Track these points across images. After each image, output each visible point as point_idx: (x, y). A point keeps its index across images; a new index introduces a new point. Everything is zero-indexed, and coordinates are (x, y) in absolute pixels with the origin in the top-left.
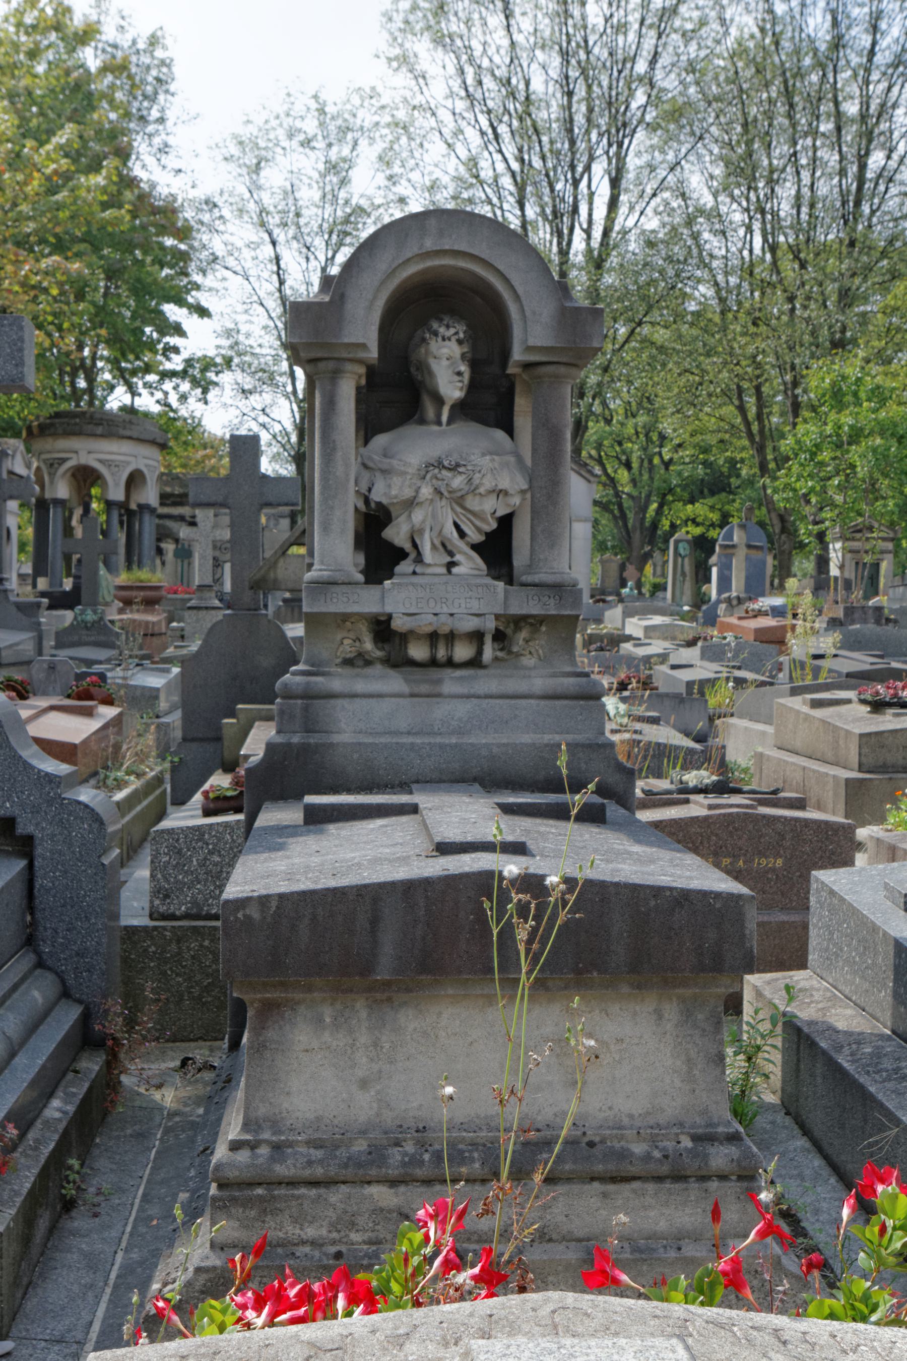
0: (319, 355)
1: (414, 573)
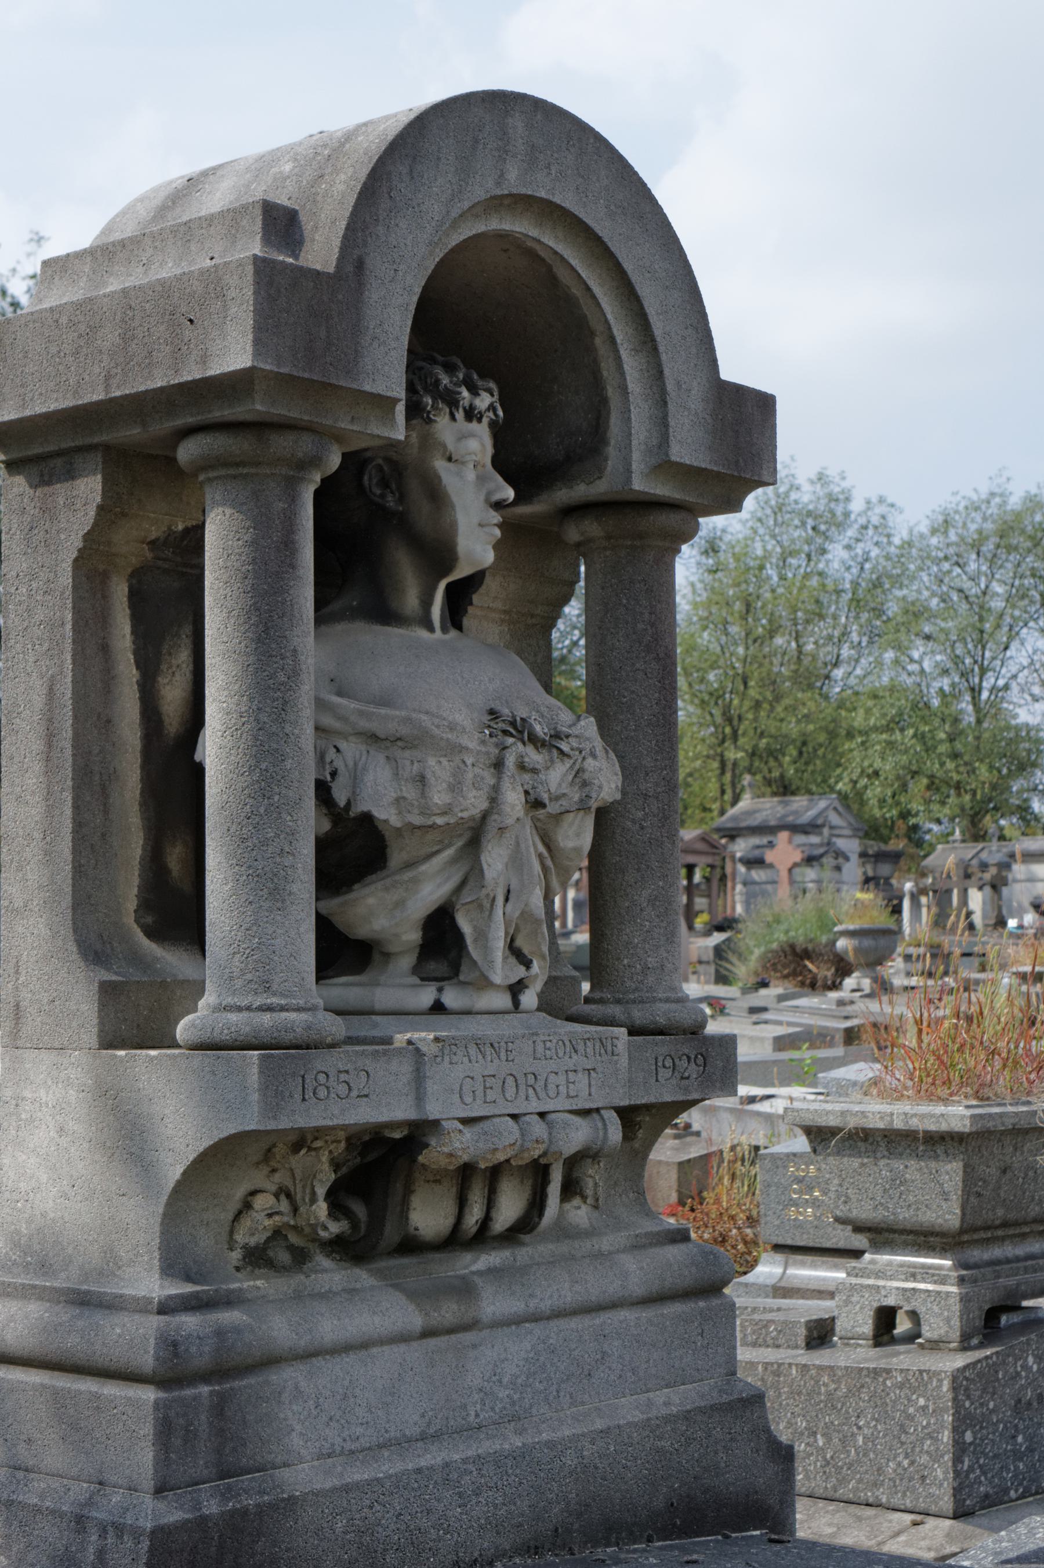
0: (294, 414)
1: (438, 1008)
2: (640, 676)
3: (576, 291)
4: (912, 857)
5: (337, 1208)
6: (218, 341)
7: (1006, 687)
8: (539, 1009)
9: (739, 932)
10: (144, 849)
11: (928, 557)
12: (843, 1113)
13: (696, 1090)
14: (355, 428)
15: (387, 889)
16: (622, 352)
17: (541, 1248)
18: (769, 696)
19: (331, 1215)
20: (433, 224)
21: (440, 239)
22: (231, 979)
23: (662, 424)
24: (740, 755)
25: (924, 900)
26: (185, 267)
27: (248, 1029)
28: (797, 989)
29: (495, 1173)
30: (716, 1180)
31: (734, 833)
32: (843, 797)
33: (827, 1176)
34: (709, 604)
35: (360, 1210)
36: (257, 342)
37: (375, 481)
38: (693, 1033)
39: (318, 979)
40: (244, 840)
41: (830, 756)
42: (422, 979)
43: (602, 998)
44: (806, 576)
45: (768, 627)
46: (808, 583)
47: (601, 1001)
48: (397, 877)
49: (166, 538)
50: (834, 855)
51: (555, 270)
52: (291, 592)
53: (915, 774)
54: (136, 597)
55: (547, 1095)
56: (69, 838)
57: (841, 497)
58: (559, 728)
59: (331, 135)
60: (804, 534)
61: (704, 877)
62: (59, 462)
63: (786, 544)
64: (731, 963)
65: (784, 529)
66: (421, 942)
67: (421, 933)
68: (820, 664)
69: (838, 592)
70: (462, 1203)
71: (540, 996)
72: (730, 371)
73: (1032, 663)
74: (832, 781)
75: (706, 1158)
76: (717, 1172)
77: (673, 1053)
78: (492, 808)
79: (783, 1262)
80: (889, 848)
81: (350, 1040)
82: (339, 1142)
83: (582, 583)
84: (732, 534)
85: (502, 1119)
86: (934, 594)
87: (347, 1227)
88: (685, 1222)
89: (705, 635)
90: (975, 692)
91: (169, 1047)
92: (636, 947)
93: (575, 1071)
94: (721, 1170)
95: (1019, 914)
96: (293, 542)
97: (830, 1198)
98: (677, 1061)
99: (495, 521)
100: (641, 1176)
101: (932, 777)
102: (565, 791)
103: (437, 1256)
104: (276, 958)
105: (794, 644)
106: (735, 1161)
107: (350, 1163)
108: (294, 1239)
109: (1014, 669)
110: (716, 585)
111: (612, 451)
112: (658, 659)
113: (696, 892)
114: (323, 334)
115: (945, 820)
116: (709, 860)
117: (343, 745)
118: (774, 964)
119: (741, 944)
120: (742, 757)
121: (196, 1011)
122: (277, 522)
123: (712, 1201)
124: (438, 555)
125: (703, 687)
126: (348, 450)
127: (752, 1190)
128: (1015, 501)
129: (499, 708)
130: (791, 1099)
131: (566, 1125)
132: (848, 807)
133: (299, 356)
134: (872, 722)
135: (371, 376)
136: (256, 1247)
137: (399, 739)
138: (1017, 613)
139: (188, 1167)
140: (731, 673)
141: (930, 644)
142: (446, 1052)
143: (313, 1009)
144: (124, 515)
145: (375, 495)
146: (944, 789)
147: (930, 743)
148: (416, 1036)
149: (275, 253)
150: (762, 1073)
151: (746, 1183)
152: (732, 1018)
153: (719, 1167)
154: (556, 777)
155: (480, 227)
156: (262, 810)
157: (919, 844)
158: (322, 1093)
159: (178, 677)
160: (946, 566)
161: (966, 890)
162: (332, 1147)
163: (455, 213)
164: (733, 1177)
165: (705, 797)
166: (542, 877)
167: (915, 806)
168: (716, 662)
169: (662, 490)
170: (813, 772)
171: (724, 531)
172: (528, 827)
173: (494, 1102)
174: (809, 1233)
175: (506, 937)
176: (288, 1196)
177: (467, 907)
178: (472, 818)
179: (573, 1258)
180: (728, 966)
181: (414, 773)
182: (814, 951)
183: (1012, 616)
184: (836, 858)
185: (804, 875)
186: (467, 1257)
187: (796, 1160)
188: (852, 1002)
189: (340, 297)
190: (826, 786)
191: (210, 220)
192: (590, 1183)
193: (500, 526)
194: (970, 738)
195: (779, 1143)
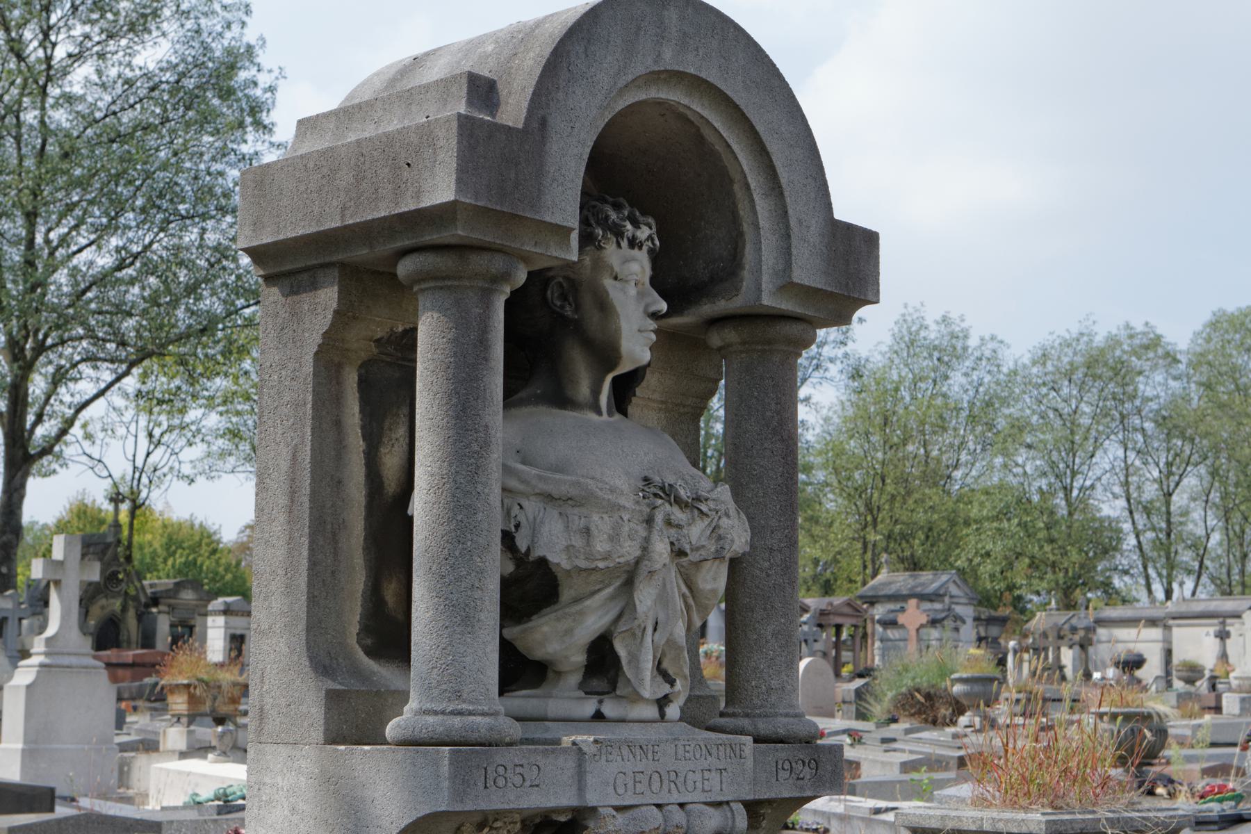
0: (488, 238)
1: (599, 716)
2: (768, 453)
3: (719, 147)
4: (1017, 622)
7: (1092, 487)
8: (681, 720)
9: (875, 678)
10: (366, 585)
11: (1030, 383)
12: (943, 818)
14: (538, 250)
15: (558, 620)
22: (430, 688)
23: (787, 252)
24: (879, 537)
25: (1026, 656)
32: (961, 572)
36: (459, 181)
39: (501, 694)
40: (442, 577)
41: (950, 540)
42: (586, 693)
44: (933, 396)
47: (734, 715)
48: (567, 610)
53: (1018, 555)
54: (364, 384)
56: (305, 574)
57: (961, 335)
59: (525, 24)
62: (305, 276)
69: (958, 410)
72: (840, 214)
73: (1113, 467)
74: (952, 559)
80: (998, 615)
86: (1034, 412)
90: (1067, 490)
95: (1104, 666)
96: (487, 340)
99: (652, 328)
101: (1032, 557)
105: (922, 451)
109: (1099, 473)
110: (861, 403)
111: (746, 274)
113: (842, 646)
114: (513, 176)
115: (1043, 593)
116: (854, 621)
117: (525, 503)
128: (1099, 340)
132: (965, 581)
134: (985, 512)
138: (1101, 428)
141: (1032, 452)
142: (604, 751)
143: (495, 714)
144: (355, 318)
146: (1042, 567)
147: (1031, 531)
154: (697, 532)
155: (642, 96)
156: (457, 553)
157: (1023, 611)
158: (501, 782)
160: (1044, 390)
161: (1059, 648)
163: (621, 84)
167: (1019, 581)
171: (867, 360)
178: (627, 563)
183: (1097, 431)
185: (929, 635)
188: (966, 735)
190: (946, 563)
191: (427, 88)
193: (655, 332)
194: (1063, 528)
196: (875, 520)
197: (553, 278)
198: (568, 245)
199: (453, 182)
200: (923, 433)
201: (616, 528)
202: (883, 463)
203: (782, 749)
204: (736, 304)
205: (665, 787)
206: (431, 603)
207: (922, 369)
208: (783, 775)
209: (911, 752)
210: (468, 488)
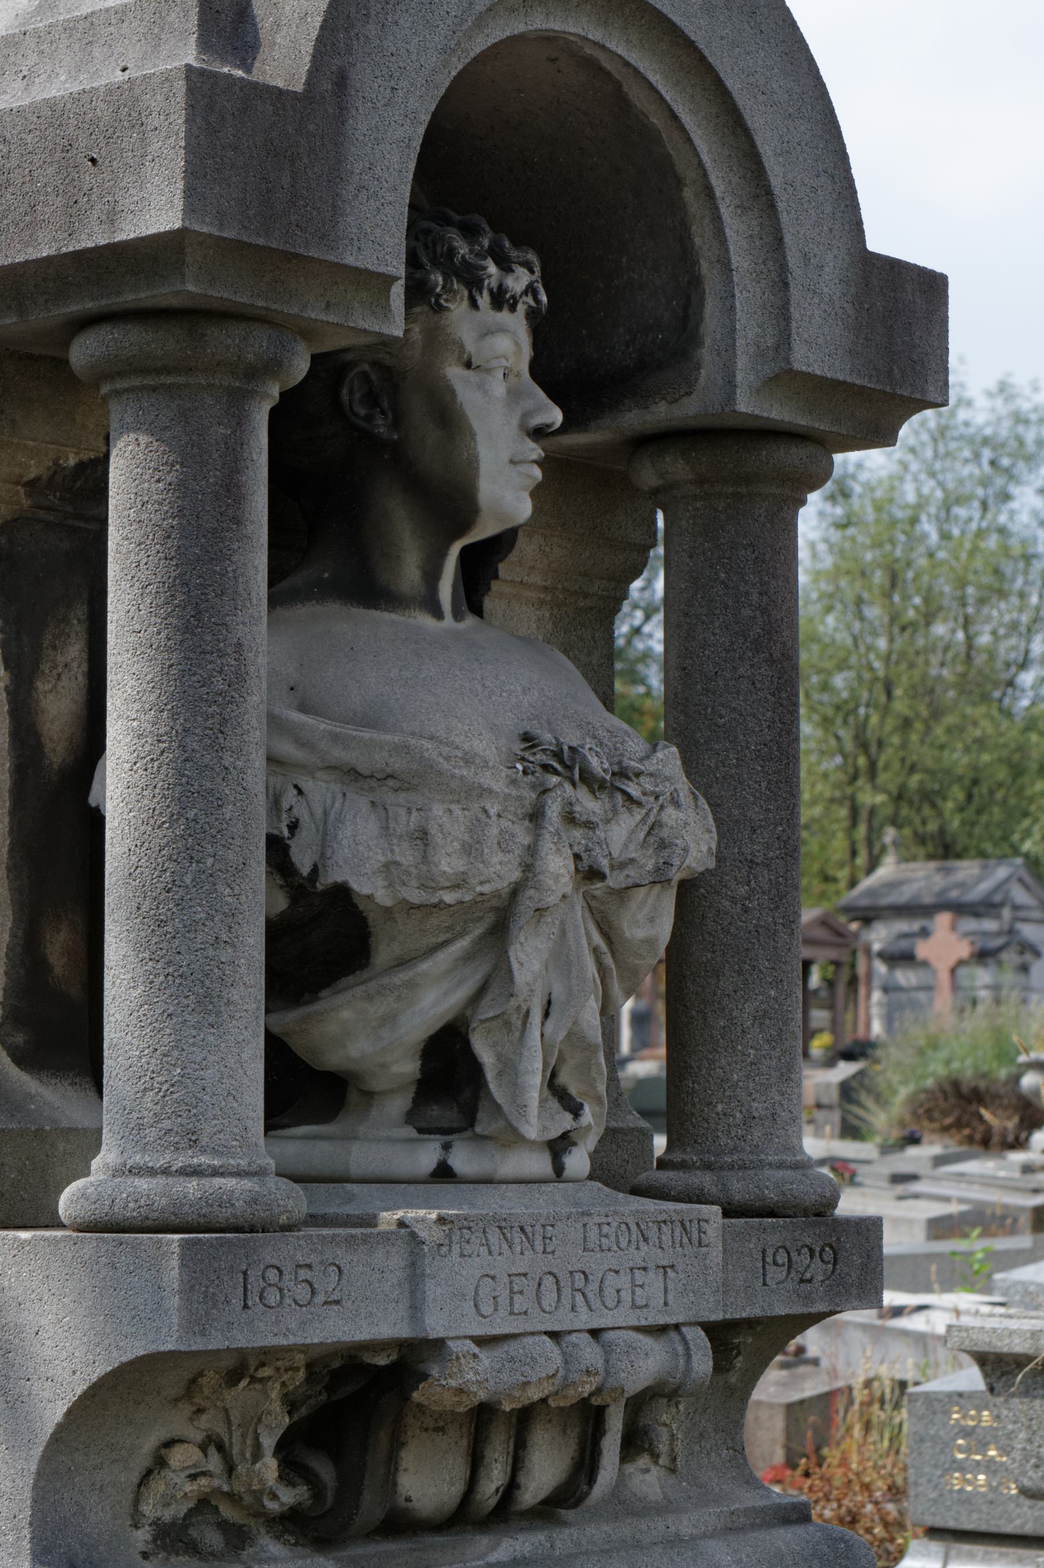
1: (443, 1173)
3: (657, 120)
5: (291, 1467)
6: (132, 191)
8: (591, 1177)
9: (877, 1061)
10: (13, 935)
13: (822, 1299)
14: (332, 318)
15: (370, 998)
16: (722, 210)
17: (590, 1530)
18: (924, 712)
19: (283, 1478)
20: (449, 22)
21: (459, 43)
22: (140, 1127)
24: (880, 798)
26: (84, 82)
27: (164, 1201)
28: (964, 1148)
29: (525, 1418)
30: (842, 1430)
31: (871, 914)
33: (1010, 1427)
34: (837, 572)
35: (325, 1471)
36: (189, 193)
37: (357, 396)
38: (818, 1215)
40: (161, 924)
41: (1013, 801)
42: (420, 1131)
43: (683, 1161)
44: (980, 534)
45: (923, 609)
46: (982, 545)
47: (683, 1166)
48: (385, 981)
49: (51, 478)
50: (1019, 948)
51: (625, 88)
52: (234, 559)
55: (604, 1304)
58: (626, 762)
60: (977, 472)
61: (824, 979)
63: (951, 486)
64: (864, 1107)
65: (948, 463)
66: (419, 1076)
67: (420, 1062)
68: (999, 665)
70: (476, 1462)
71: (593, 1156)
72: (879, 241)
74: (1016, 837)
75: (827, 1399)
76: (844, 1418)
77: (788, 1244)
78: (527, 879)
79: (941, 1555)
81: (314, 1220)
82: (298, 1369)
83: (660, 550)
84: (871, 471)
85: (537, 1338)
87: (306, 1495)
88: (795, 1492)
89: (830, 620)
91: (47, 1227)
92: (736, 1086)
93: (645, 1269)
94: (850, 1415)
96: (238, 486)
97: (1014, 1460)
98: (794, 1255)
99: (534, 456)
100: (738, 1424)
102: (633, 855)
103: (438, 1539)
104: (207, 1098)
105: (960, 635)
106: (869, 1404)
107: (312, 1401)
108: (227, 1511)
110: (847, 545)
111: (706, 355)
112: (771, 661)
114: (286, 180)
116: (832, 954)
117: (307, 784)
118: (929, 1112)
119: (880, 1079)
120: (883, 804)
121: (87, 1174)
122: (215, 456)
123: (836, 1462)
124: (450, 504)
125: (826, 697)
126: (318, 351)
127: (895, 1446)
129: (538, 731)
130: (957, 1312)
131: (631, 1347)
133: (251, 213)
135: (356, 243)
136: (173, 1523)
137: (391, 776)
139: (75, 1403)
140: (867, 676)
142: (455, 1238)
143: (259, 1173)
145: (357, 415)
148: (410, 1214)
149: (217, 63)
150: (919, 1274)
151: (887, 1435)
152: (866, 1190)
153: (846, 1411)
154: (621, 834)
155: (517, 26)
158: (273, 1297)
159: (65, 681)
162: (285, 1377)
164: (867, 1426)
165: (826, 861)
166: (598, 981)
168: (845, 660)
169: (778, 412)
170: (988, 825)
172: (578, 909)
173: (525, 1313)
174: (980, 1512)
175: (544, 1071)
176: (221, 1448)
177: (487, 1024)
178: (496, 894)
179: (638, 1545)
180: (860, 1112)
181: (412, 826)
182: (987, 1091)
184: (1022, 953)
186: (483, 1541)
187: (962, 1402)
189: (312, 127)
192: (664, 1434)
195: (935, 1377)
196: (872, 766)
197: (352, 364)
198: (386, 309)
199: (179, 194)
200: (963, 602)
201: (477, 827)
202: (887, 659)
203: (773, 1227)
204: (687, 410)
205: (566, 1301)
206: (140, 971)
207: (961, 482)
208: (776, 1274)
209: (961, 1201)
210: (207, 759)
